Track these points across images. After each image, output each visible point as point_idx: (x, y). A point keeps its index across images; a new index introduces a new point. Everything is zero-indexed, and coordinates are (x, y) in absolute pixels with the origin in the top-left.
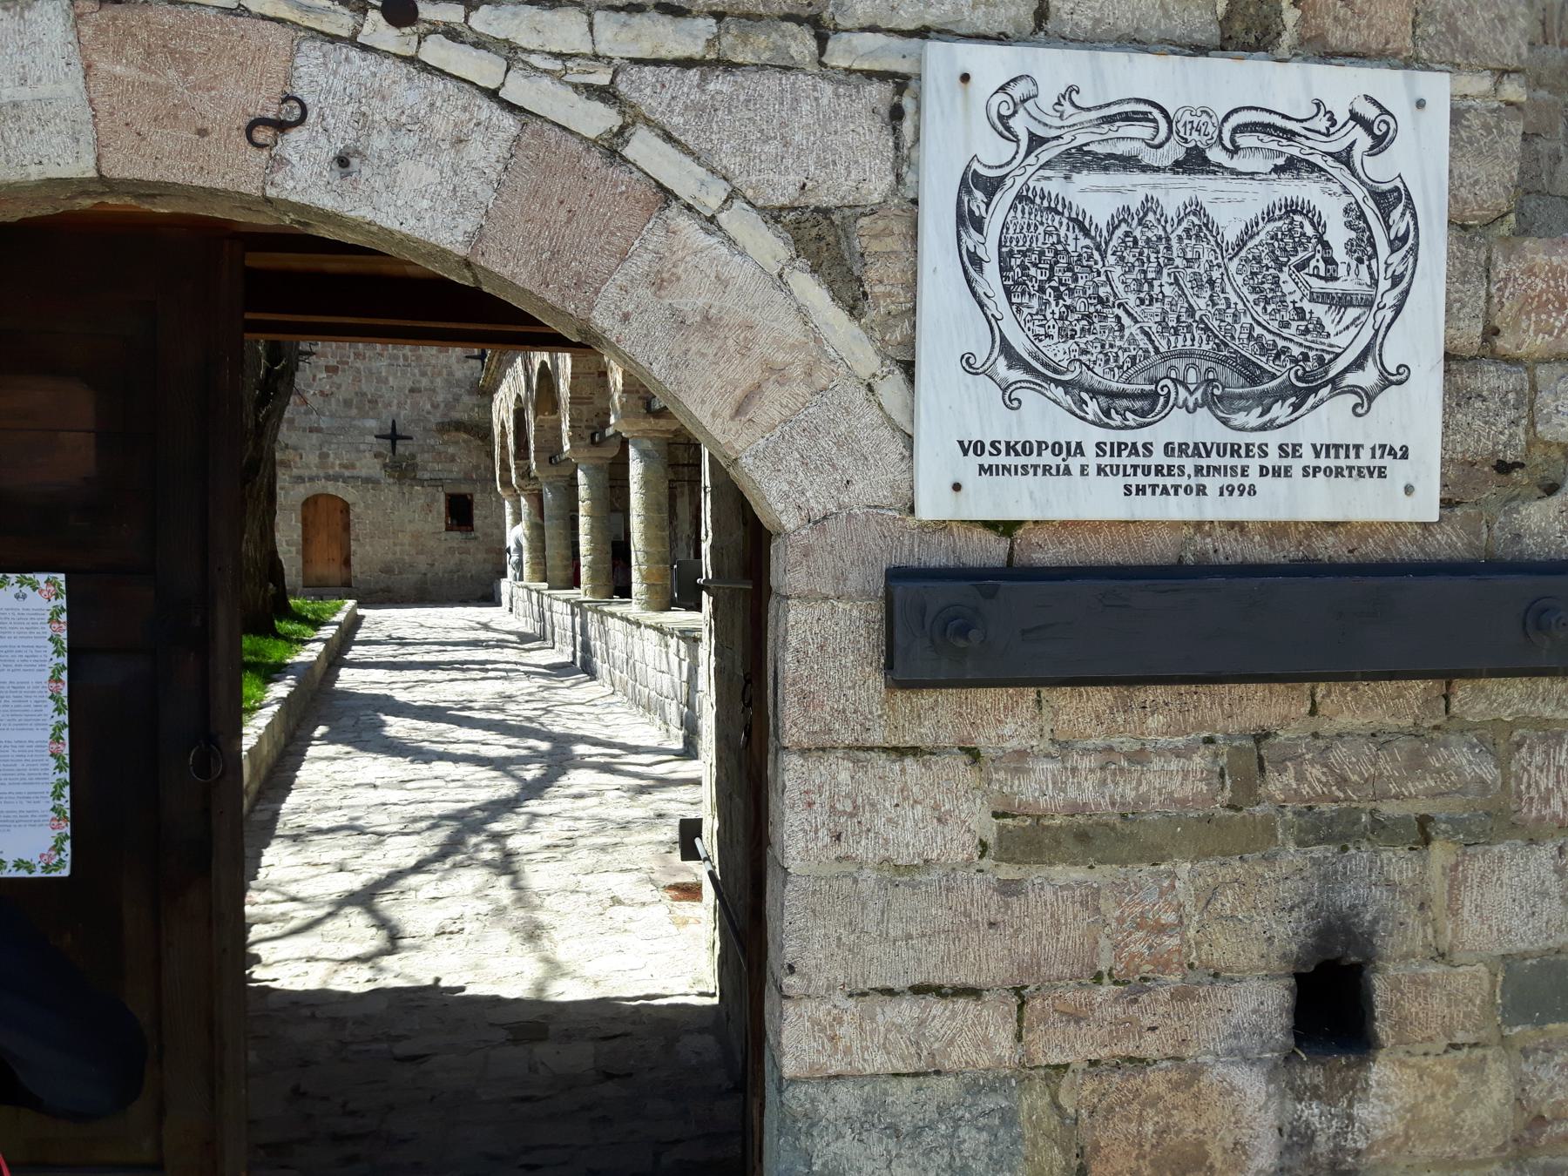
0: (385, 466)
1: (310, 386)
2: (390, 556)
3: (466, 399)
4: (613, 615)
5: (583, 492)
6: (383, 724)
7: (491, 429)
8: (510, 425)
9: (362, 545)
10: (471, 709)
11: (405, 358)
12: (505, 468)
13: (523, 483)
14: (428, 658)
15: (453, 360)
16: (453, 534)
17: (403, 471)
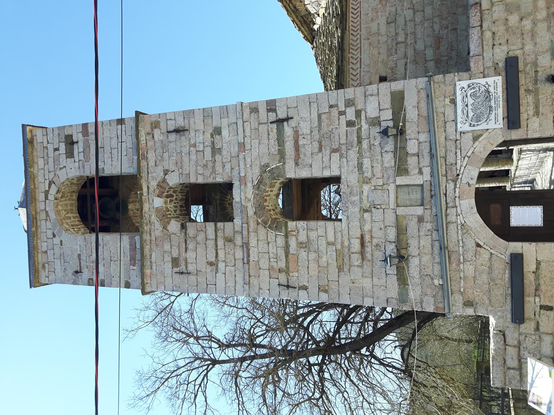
4: (515, 174)
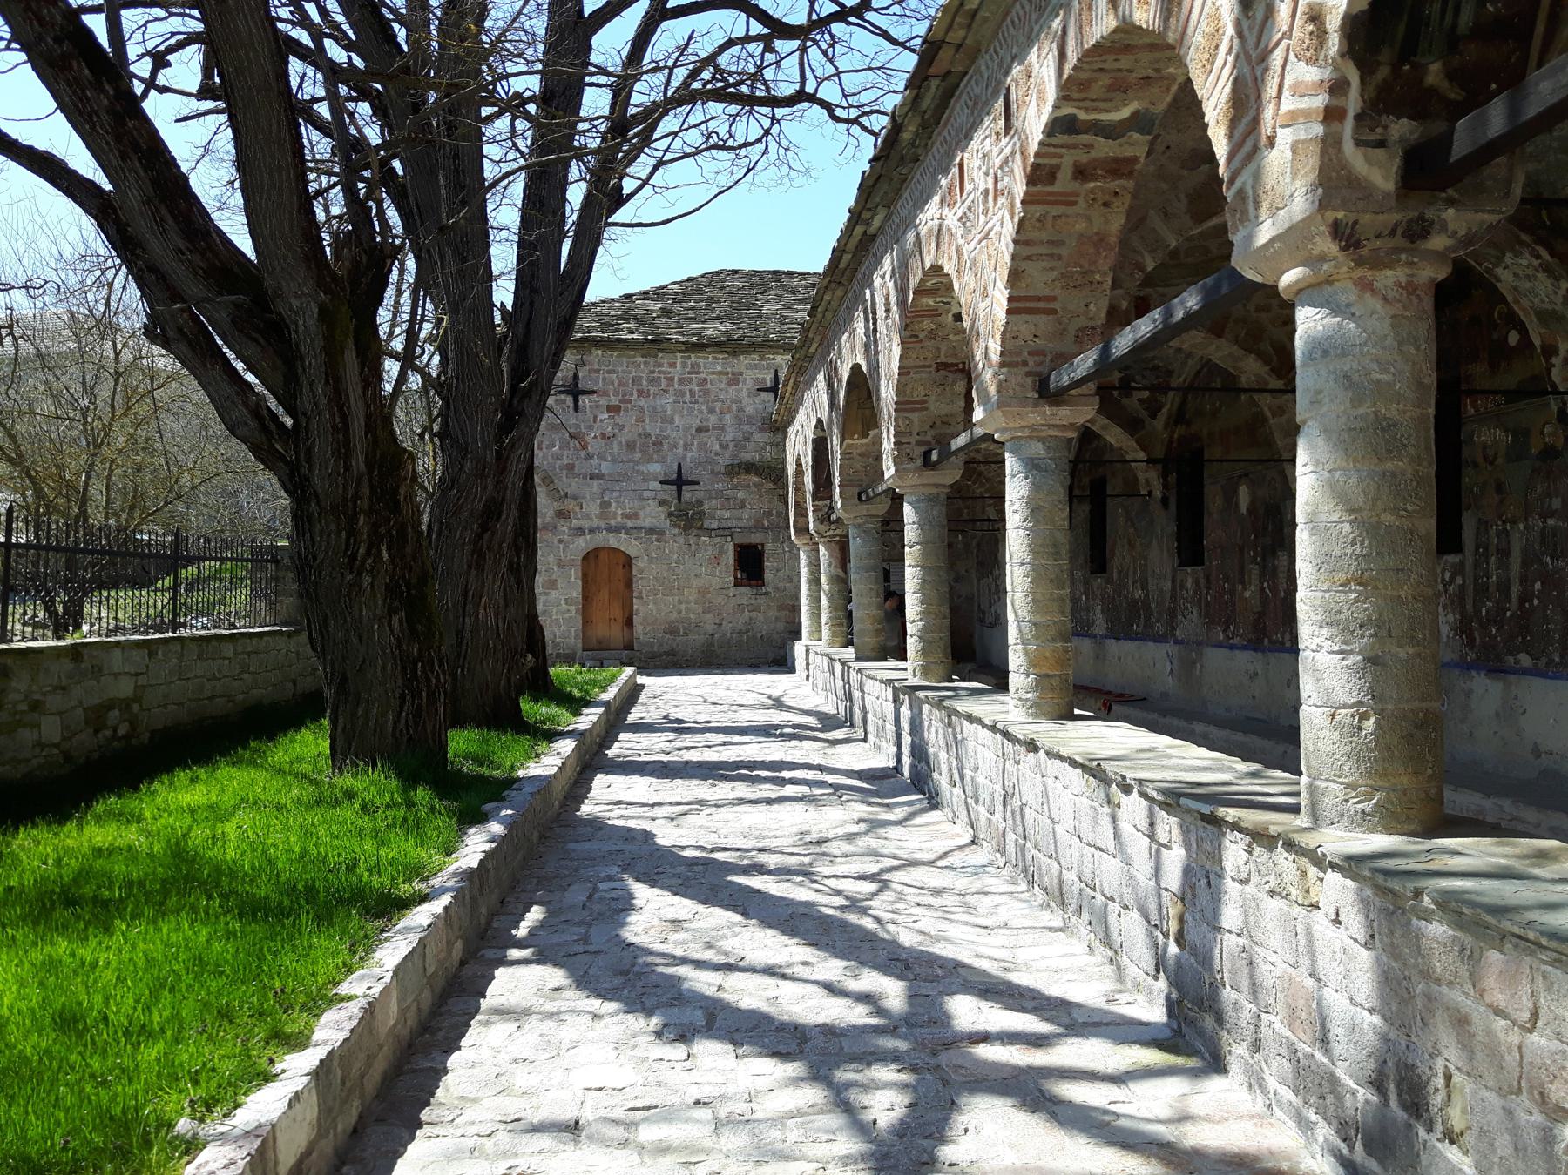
0: (670, 514)
1: (590, 428)
2: (674, 616)
3: (758, 437)
4: (970, 718)
5: (910, 534)
6: (626, 905)
7: (784, 470)
8: (808, 460)
9: (646, 603)
10: (760, 870)
11: (692, 393)
12: (801, 512)
13: (823, 528)
14: (711, 756)
15: (744, 393)
16: (742, 589)
17: (688, 519)
